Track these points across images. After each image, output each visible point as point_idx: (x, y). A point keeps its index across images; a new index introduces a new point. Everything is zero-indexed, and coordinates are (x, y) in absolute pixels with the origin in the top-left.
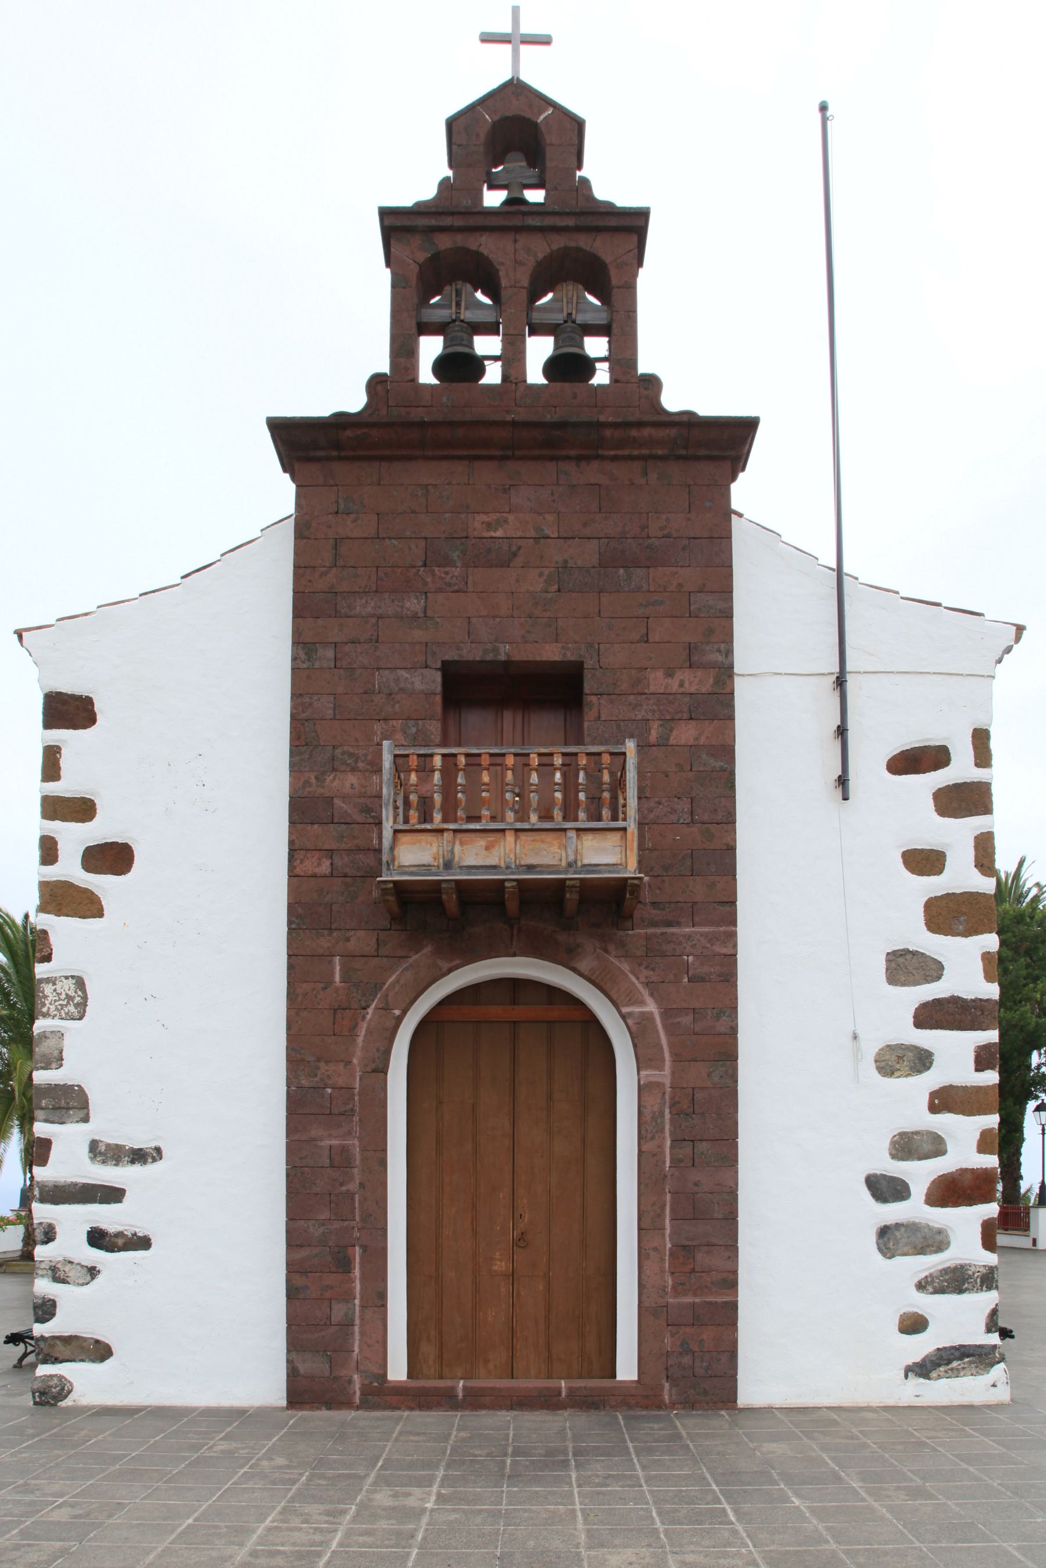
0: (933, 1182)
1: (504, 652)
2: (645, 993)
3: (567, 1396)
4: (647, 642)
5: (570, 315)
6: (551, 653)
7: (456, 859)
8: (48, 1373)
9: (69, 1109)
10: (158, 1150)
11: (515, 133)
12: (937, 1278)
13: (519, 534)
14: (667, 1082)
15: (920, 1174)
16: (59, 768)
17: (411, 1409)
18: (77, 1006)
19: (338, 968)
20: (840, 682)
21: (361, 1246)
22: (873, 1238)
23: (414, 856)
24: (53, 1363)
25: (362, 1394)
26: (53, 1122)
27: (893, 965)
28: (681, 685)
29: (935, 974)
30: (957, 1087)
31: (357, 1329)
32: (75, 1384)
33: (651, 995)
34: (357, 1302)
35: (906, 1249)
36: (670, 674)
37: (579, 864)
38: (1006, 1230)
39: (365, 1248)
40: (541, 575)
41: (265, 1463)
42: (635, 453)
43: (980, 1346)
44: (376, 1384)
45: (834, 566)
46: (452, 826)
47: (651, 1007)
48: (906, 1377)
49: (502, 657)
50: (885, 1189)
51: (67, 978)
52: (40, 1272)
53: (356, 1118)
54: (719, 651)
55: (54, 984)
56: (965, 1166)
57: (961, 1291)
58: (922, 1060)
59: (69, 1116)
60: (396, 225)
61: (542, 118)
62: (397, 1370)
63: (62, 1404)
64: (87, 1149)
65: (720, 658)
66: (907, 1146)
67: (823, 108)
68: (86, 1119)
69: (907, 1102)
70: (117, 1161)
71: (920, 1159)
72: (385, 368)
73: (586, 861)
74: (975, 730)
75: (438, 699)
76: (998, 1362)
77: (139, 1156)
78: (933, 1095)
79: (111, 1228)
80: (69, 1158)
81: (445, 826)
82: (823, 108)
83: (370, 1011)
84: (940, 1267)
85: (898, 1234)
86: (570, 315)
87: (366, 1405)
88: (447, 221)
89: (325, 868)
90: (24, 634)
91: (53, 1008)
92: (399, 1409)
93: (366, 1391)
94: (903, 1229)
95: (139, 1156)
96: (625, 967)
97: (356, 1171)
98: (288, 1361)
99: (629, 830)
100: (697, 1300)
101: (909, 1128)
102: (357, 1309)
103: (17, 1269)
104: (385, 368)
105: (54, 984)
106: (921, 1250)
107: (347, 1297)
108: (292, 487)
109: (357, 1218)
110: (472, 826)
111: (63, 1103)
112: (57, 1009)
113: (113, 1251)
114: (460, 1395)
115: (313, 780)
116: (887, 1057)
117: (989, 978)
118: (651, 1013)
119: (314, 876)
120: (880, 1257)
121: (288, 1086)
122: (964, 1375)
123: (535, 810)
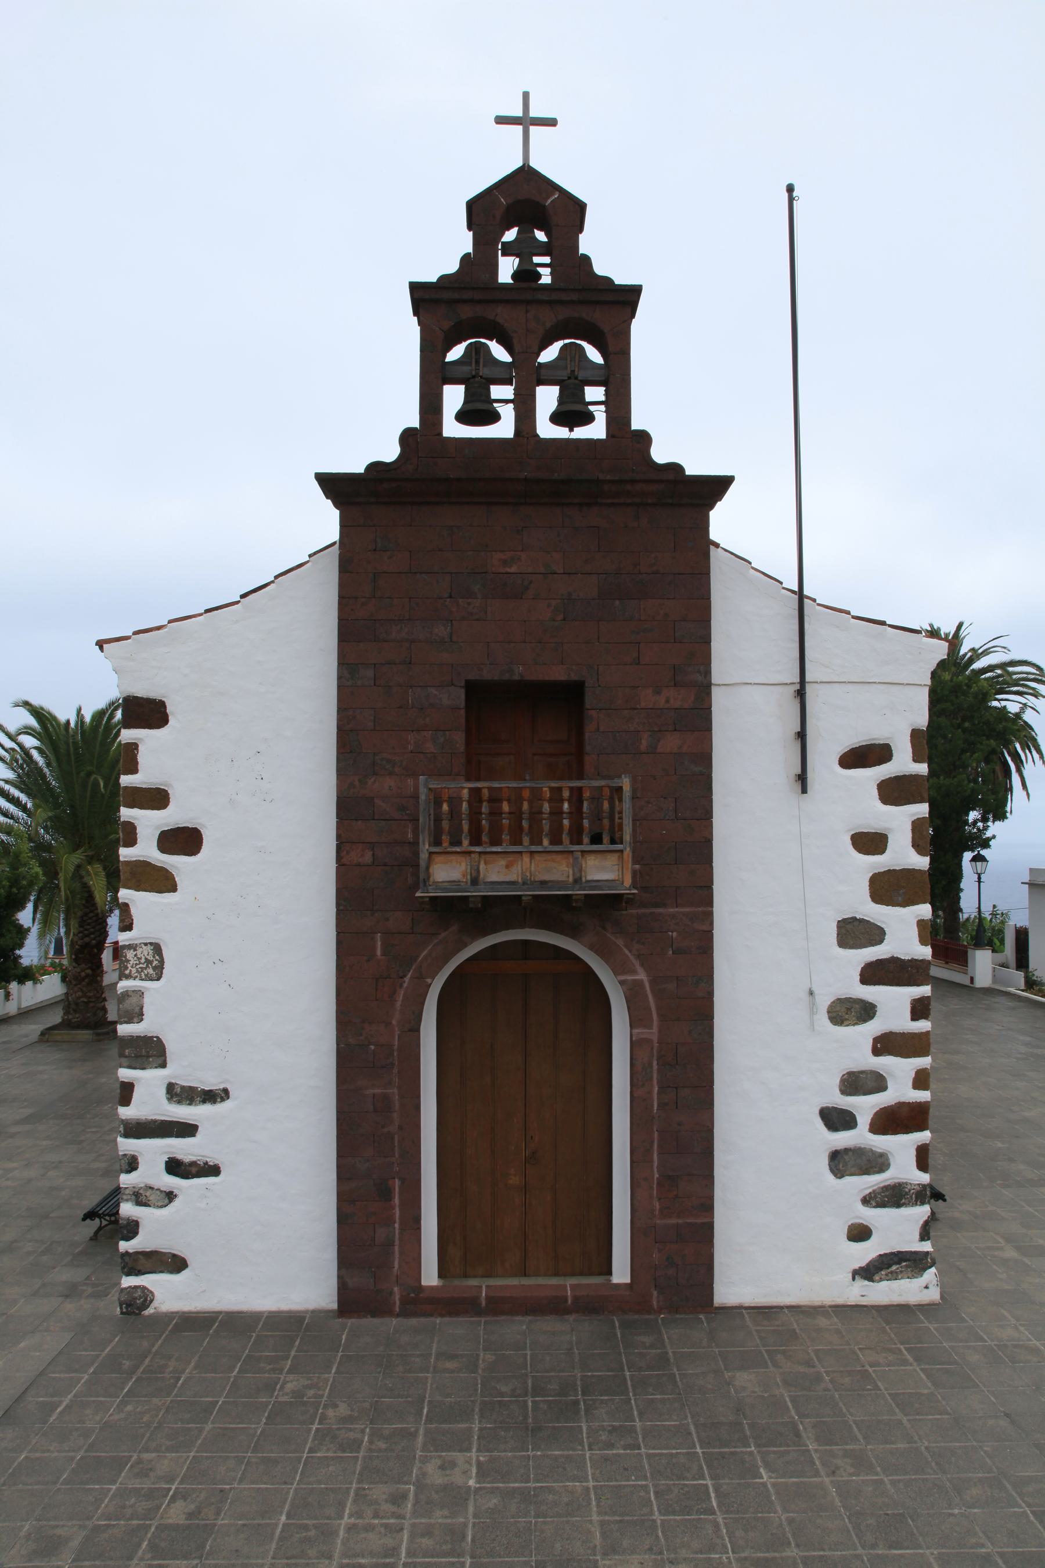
0: (876, 1114)
1: (519, 672)
2: (637, 963)
3: (572, 1303)
4: (638, 664)
5: (573, 371)
6: (558, 674)
7: (482, 876)
8: (133, 1284)
9: (148, 1057)
10: (226, 1091)
11: (526, 208)
12: (879, 1194)
13: (530, 570)
14: (655, 1039)
15: (865, 1107)
16: (137, 763)
17: (442, 1316)
18: (155, 968)
19: (379, 943)
20: (801, 693)
21: (399, 1179)
22: (826, 1161)
23: (447, 873)
24: (137, 1275)
25: (401, 1303)
26: (135, 1068)
27: (843, 931)
28: (667, 701)
29: (878, 938)
30: (896, 1033)
31: (397, 1248)
32: (156, 1293)
33: (642, 965)
34: (397, 1225)
35: (853, 1170)
36: (658, 692)
37: (584, 879)
38: (947, 963)
39: (403, 1181)
40: (549, 606)
41: (330, 1413)
42: (629, 501)
43: (916, 1253)
44: (412, 1295)
45: (796, 589)
46: (478, 849)
47: (642, 976)
48: (854, 1279)
49: (516, 677)
50: (837, 1119)
51: (146, 944)
52: (125, 1197)
53: (395, 1071)
54: (699, 672)
55: (135, 950)
56: (902, 1100)
57: (898, 1205)
58: (866, 1011)
59: (149, 1063)
60: (424, 297)
61: (549, 201)
62: (430, 1276)
63: (146, 1313)
64: (164, 1091)
65: (700, 678)
66: (856, 1083)
67: (790, 189)
68: (163, 1065)
69: (855, 1045)
70: (191, 1101)
71: (865, 1094)
72: (415, 423)
73: (589, 878)
74: (913, 730)
75: (463, 712)
76: (930, 1267)
77: (211, 1097)
78: (876, 1040)
79: (187, 1158)
80: (149, 1098)
81: (472, 849)
82: (790, 189)
83: (407, 979)
84: (882, 1185)
85: (846, 1157)
86: (573, 371)
87: (405, 1313)
88: (467, 295)
89: (368, 858)
90: (105, 646)
91: (134, 970)
92: (432, 1315)
93: (405, 1301)
94: (850, 1153)
95: (211, 1097)
96: (620, 942)
97: (395, 1115)
98: (339, 1277)
99: (625, 853)
100: (680, 1221)
101: (855, 1067)
102: (397, 1232)
103: (59, 1038)
104: (415, 423)
105: (135, 950)
106: (866, 1171)
107: (389, 1221)
108: (336, 514)
109: (397, 1155)
110: (494, 849)
111: (144, 1052)
112: (137, 971)
113: (187, 1178)
114: (484, 1303)
115: (357, 783)
116: (838, 1009)
117: (923, 942)
118: (642, 981)
119: (359, 865)
120: (831, 1177)
121: (338, 1044)
122: (902, 1278)
123: (547, 835)
